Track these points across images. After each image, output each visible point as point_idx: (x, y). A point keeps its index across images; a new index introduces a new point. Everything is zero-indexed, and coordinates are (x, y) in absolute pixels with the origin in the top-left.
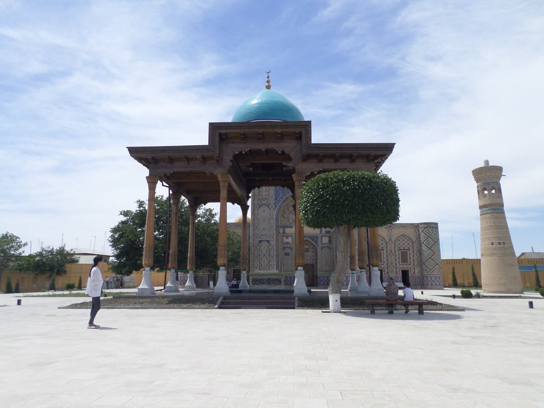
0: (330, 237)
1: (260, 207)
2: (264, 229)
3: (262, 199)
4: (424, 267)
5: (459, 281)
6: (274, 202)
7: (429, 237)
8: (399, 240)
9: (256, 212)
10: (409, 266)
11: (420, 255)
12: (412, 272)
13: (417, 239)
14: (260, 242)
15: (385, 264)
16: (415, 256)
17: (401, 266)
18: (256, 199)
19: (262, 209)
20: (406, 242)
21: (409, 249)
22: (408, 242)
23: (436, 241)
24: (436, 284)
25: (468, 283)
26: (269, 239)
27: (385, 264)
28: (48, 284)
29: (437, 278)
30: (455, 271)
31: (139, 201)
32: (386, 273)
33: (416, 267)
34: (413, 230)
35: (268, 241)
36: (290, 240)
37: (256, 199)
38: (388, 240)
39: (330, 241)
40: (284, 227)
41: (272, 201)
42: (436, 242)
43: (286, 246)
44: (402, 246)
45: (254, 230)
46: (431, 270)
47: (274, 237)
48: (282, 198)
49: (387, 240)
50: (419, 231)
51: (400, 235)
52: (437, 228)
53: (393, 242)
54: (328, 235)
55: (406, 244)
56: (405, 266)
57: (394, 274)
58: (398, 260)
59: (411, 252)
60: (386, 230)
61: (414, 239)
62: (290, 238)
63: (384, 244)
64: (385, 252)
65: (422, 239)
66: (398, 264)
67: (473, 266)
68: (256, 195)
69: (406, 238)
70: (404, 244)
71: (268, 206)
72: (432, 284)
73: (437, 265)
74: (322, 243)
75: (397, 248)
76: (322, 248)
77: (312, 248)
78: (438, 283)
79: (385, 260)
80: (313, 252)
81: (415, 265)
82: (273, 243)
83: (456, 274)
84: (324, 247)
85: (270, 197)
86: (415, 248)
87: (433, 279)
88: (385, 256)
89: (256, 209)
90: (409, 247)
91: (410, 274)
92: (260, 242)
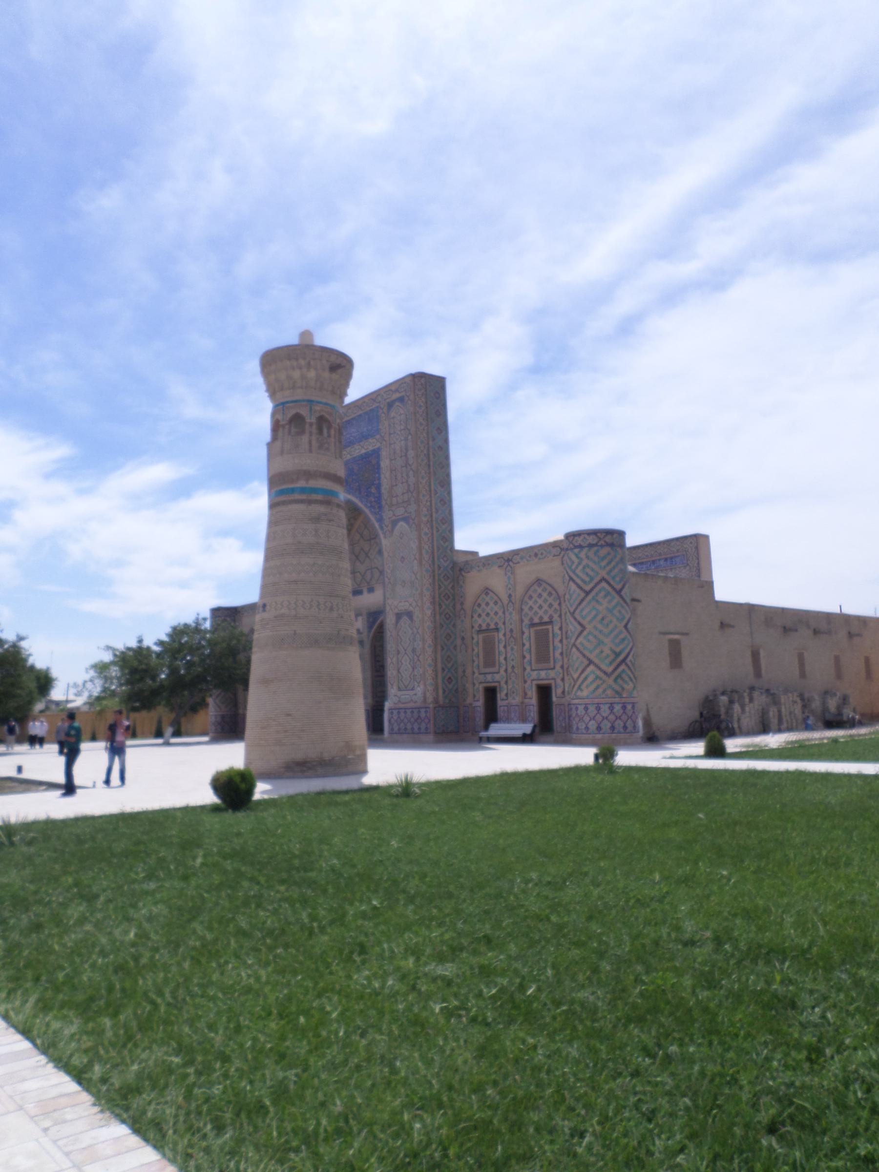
8: (531, 597)
12: (559, 691)
17: (534, 674)
24: (587, 728)
28: (240, 687)
31: (87, 669)
34: (557, 563)
44: (536, 613)
56: (543, 674)
66: (528, 668)
69: (545, 590)
73: (592, 667)
75: (526, 621)
78: (593, 725)
90: (551, 617)
91: (554, 699)
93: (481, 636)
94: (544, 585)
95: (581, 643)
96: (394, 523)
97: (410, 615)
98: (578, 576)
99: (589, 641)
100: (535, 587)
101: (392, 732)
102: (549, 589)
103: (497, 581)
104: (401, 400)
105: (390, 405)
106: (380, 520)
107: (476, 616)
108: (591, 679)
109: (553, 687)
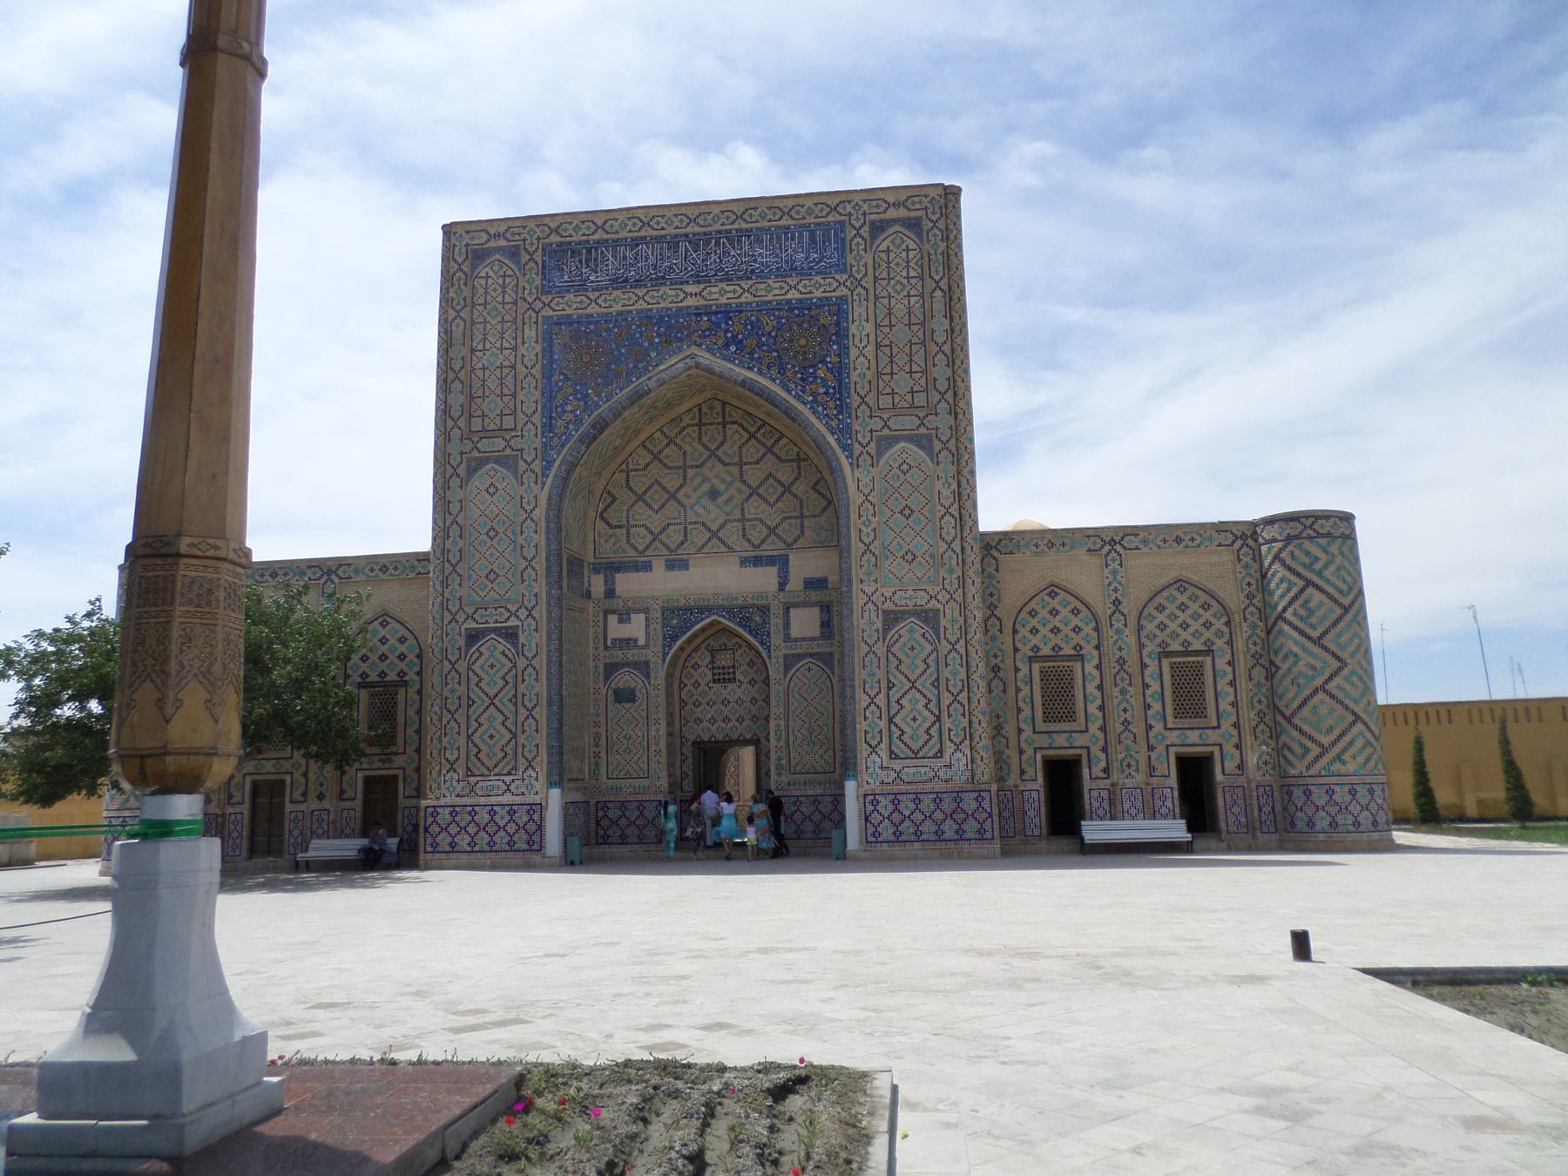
0: (826, 608)
1: (471, 471)
2: (492, 576)
3: (485, 433)
4: (1292, 737)
5: (1444, 796)
6: (538, 443)
7: (1309, 583)
8: (1161, 608)
9: (455, 494)
10: (1213, 736)
11: (1270, 676)
12: (1230, 765)
13: (1250, 597)
14: (473, 637)
15: (1094, 728)
16: (1243, 683)
17: (1173, 737)
18: (456, 433)
19: (480, 481)
20: (1196, 617)
21: (1209, 652)
22: (1207, 616)
23: (1351, 604)
24: (1356, 823)
25: (1480, 802)
26: (513, 622)
27: (1094, 728)
29: (1362, 793)
30: (1427, 755)
32: (1097, 772)
33: (1248, 739)
34: (1226, 557)
35: (511, 635)
36: (636, 628)
37: (456, 433)
38: (1103, 608)
39: (826, 625)
40: (611, 569)
41: (530, 441)
42: (1346, 610)
43: (618, 655)
44: (1174, 636)
45: (445, 583)
46: (1325, 750)
47: (541, 612)
48: (578, 422)
49: (1099, 610)
50: (1257, 557)
51: (1164, 580)
52: (1349, 537)
53: (1132, 620)
54: (815, 596)
55: (1195, 626)
56: (1193, 737)
57: (1140, 778)
58: (1157, 706)
59: (1221, 664)
60: (1096, 561)
61: (1235, 601)
62: (638, 620)
63: (1088, 629)
64: (1090, 667)
65: (1279, 592)
66: (1158, 727)
67: (1503, 729)
68: (455, 413)
69: (1193, 598)
70: (1185, 626)
71: (509, 462)
72: (1334, 824)
73: (1359, 726)
74: (787, 638)
75: (1151, 647)
76: (790, 661)
77: (751, 664)
78: (1365, 818)
79: (1093, 709)
80: (752, 682)
81: (1246, 727)
82: (535, 639)
83: (1429, 768)
84: (799, 657)
85: (522, 418)
86: (1240, 644)
87: (1341, 795)
88: (1091, 688)
89: (455, 482)
91: (1219, 777)
92: (473, 637)
93: (1036, 667)
94: (1191, 589)
95: (1338, 687)
96: (885, 443)
97: (930, 618)
98: (1328, 581)
99: (1353, 684)
100: (1044, 595)
101: (872, 837)
102: (1204, 597)
103: (1085, 577)
104: (914, 225)
105: (878, 228)
106: (845, 434)
107: (1023, 632)
108: (1360, 743)
109: (1084, 762)
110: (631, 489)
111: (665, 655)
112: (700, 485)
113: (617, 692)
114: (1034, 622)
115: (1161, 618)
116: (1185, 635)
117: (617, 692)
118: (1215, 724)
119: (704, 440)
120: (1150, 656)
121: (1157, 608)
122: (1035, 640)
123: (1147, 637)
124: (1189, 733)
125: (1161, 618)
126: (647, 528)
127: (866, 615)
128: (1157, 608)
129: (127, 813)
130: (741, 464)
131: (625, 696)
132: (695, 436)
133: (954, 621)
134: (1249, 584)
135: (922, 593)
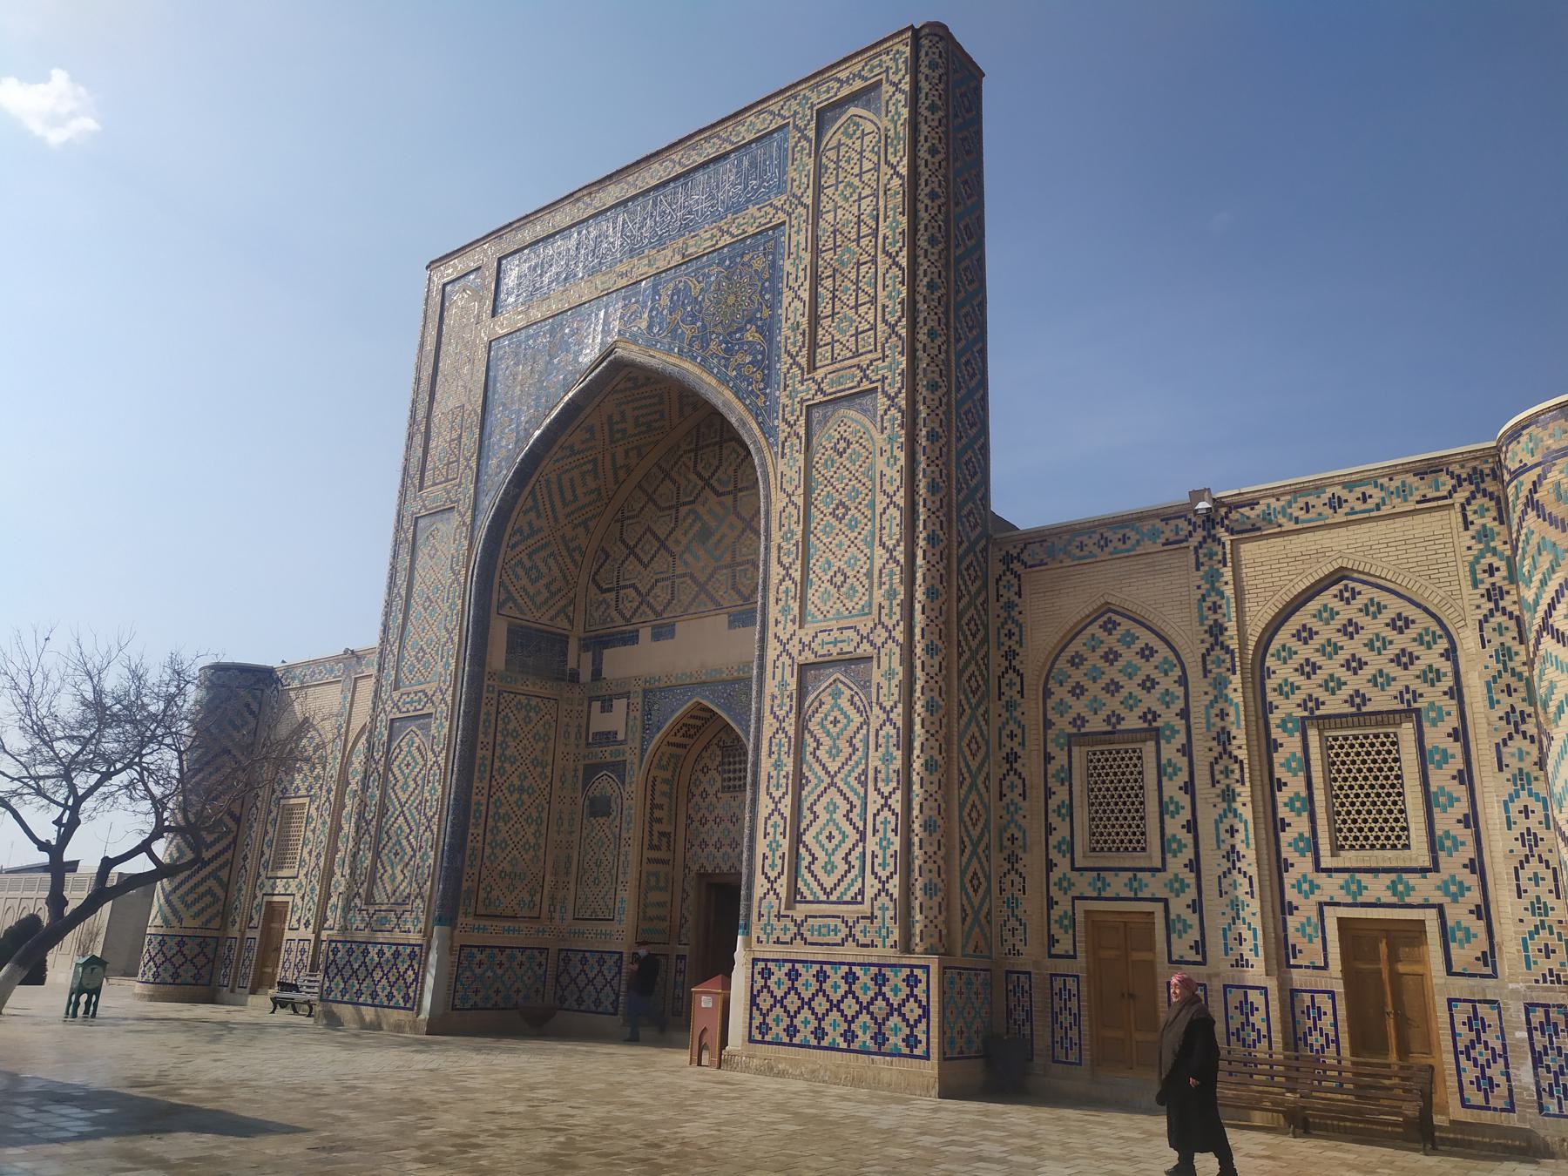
40: (598, 643)
102: (1394, 606)
106: (763, 415)
107: (1061, 693)
110: (624, 542)
111: (643, 751)
112: (691, 526)
113: (592, 801)
114: (1077, 675)
115: (1306, 652)
116: (1355, 682)
117: (592, 801)
118: (1425, 861)
119: (699, 468)
120: (1283, 725)
121: (1297, 635)
122: (1079, 706)
123: (1279, 689)
124: (1365, 878)
125: (1306, 652)
126: (636, 589)
127: (778, 672)
128: (1297, 635)
129: (208, 933)
130: (707, 483)
131: (600, 808)
132: (691, 464)
133: (890, 674)
134: (1491, 570)
135: (851, 633)
